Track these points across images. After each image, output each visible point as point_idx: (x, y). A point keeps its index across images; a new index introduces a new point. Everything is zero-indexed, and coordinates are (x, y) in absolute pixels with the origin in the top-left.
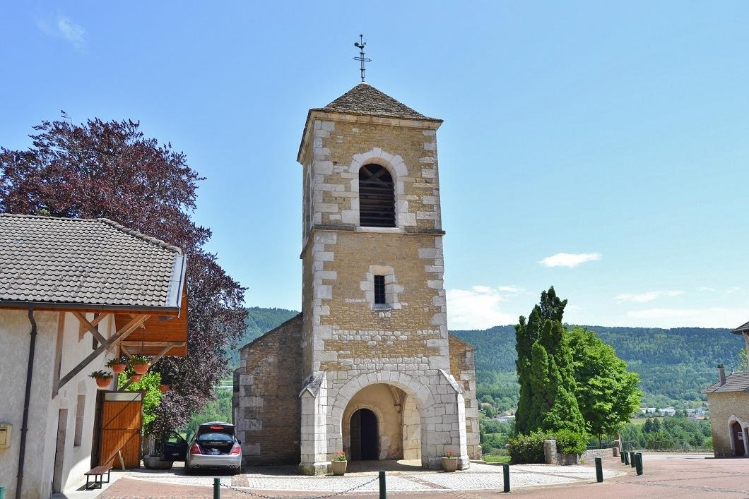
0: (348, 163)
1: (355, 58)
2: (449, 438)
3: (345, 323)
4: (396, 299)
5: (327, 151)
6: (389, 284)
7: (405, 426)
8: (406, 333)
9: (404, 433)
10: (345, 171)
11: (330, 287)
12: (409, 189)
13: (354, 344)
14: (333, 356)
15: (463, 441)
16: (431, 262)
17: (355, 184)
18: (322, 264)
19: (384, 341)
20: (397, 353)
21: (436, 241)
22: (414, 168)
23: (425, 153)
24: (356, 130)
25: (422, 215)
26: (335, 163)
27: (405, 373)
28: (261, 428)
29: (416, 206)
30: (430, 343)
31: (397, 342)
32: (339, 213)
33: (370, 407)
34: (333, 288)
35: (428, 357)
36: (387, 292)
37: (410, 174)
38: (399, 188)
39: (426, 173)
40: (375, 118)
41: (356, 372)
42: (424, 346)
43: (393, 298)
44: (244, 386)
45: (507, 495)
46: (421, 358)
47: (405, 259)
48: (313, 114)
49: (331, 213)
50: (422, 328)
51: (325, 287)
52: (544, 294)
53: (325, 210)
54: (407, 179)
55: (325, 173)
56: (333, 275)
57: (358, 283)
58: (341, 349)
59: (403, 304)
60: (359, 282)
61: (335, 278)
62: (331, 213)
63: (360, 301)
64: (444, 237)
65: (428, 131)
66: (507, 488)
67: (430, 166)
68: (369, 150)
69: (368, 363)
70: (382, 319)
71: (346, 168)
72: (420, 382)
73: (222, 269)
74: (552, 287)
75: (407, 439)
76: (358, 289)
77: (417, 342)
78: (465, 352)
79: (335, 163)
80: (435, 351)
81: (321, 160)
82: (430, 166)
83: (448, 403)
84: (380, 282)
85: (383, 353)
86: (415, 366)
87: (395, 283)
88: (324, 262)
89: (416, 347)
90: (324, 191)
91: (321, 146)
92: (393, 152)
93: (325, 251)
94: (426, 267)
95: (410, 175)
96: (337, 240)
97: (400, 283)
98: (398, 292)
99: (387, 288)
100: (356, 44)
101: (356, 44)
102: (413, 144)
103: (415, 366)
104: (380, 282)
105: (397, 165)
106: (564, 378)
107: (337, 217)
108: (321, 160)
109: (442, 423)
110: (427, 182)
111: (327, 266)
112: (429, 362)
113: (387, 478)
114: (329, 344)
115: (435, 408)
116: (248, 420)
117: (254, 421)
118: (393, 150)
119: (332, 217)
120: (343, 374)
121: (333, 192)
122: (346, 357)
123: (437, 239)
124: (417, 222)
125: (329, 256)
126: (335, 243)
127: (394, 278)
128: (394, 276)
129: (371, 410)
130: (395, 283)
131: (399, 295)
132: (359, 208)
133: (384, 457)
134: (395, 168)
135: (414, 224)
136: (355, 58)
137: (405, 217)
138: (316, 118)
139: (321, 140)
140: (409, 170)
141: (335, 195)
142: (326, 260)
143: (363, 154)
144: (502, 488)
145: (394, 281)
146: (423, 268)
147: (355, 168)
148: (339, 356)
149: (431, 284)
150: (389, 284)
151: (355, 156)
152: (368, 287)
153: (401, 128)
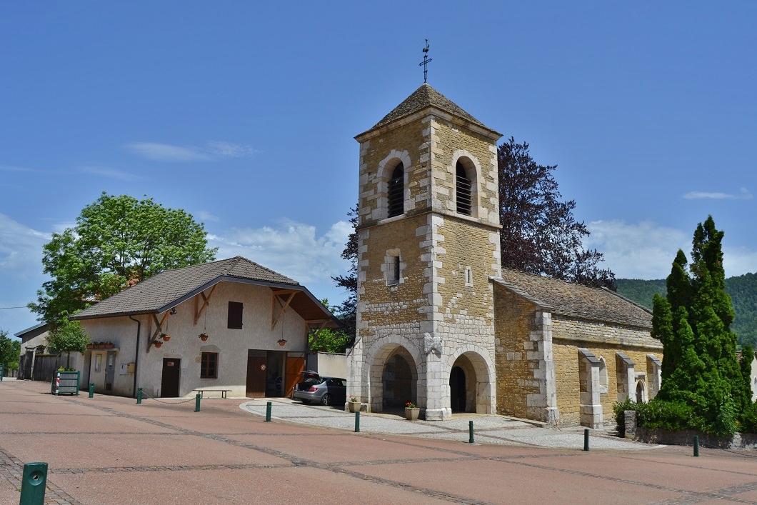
3: (373, 298)
8: (407, 303)
13: (377, 314)
15: (493, 392)
19: (393, 310)
20: (400, 320)
24: (381, 141)
25: (419, 198)
26: (369, 174)
30: (420, 310)
31: (401, 311)
32: (371, 213)
35: (419, 322)
40: (389, 126)
41: (377, 336)
42: (417, 312)
45: (268, 424)
50: (416, 298)
52: (700, 226)
56: (443, 251)
58: (370, 319)
66: (357, 429)
69: (383, 329)
70: (392, 293)
74: (710, 219)
75: (478, 395)
77: (413, 310)
78: (535, 312)
79: (369, 174)
85: (392, 320)
86: (410, 330)
103: (410, 330)
106: (697, 335)
111: (439, 243)
113: (361, 418)
117: (390, 373)
120: (370, 338)
125: (442, 238)
137: (409, 204)
144: (582, 446)
149: (423, 258)
153: (408, 125)
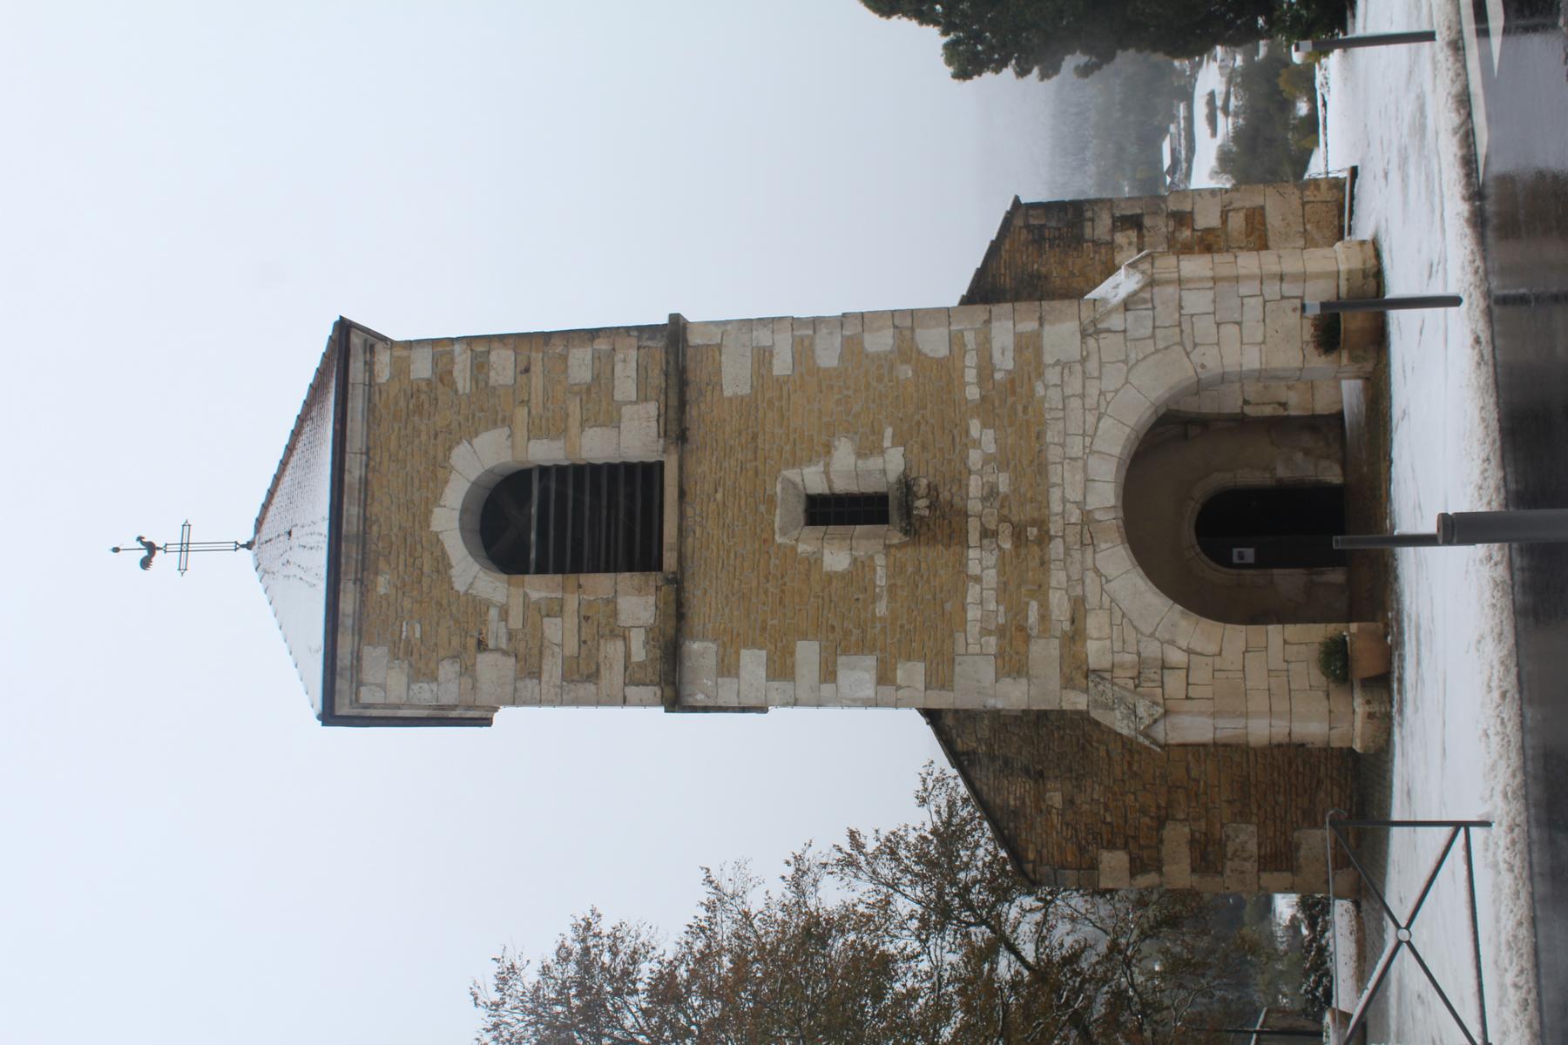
0: (479, 607)
1: (183, 570)
2: (1284, 303)
4: (875, 463)
5: (447, 670)
6: (829, 481)
7: (1248, 410)
9: (1268, 411)
10: (504, 614)
11: (841, 660)
12: (552, 427)
14: (1045, 653)
16: (763, 357)
17: (539, 588)
18: (776, 684)
21: (699, 342)
22: (486, 409)
23: (444, 376)
24: (382, 584)
26: (481, 645)
27: (1093, 437)
28: (1252, 828)
29: (599, 403)
30: (1005, 362)
33: (1192, 510)
34: (846, 652)
36: (853, 488)
37: (504, 420)
38: (546, 452)
39: (503, 366)
42: (1012, 383)
43: (869, 473)
44: (1132, 875)
46: (1048, 391)
47: (755, 437)
48: (343, 709)
49: (627, 655)
51: (842, 675)
53: (619, 679)
54: (521, 433)
55: (511, 674)
57: (831, 577)
59: (887, 443)
60: (828, 574)
61: (815, 645)
62: (627, 655)
63: (880, 572)
64: (691, 317)
65: (377, 368)
67: (480, 366)
68: (437, 541)
71: (493, 613)
72: (1117, 391)
73: (950, 70)
75: (1284, 405)
76: (846, 577)
79: (481, 645)
80: (1029, 347)
81: (474, 688)
82: (480, 366)
83: (1181, 307)
84: (826, 511)
87: (827, 465)
88: (770, 678)
89: (1013, 401)
90: (563, 678)
91: (434, 686)
92: (441, 473)
93: (737, 676)
94: (776, 372)
95: (508, 421)
96: (704, 638)
97: (828, 448)
98: (852, 459)
99: (842, 486)
100: (145, 563)
101: (145, 563)
102: (419, 409)
104: (826, 511)
105: (482, 456)
107: (637, 640)
108: (474, 688)
109: (1239, 324)
110: (527, 370)
112: (1058, 362)
114: (1012, 664)
115: (1195, 345)
116: (1229, 863)
118: (438, 471)
119: (639, 653)
121: (567, 653)
122: (1044, 617)
123: (694, 339)
124: (646, 400)
126: (712, 647)
127: (813, 469)
128: (806, 471)
129: (1199, 506)
130: (827, 465)
131: (860, 455)
132: (612, 575)
133: (1337, 469)
134: (473, 478)
135: (652, 408)
136: (183, 570)
138: (356, 700)
139: (415, 687)
140: (495, 424)
141: (572, 647)
142: (762, 673)
143: (453, 562)
145: (820, 467)
146: (780, 383)
147: (490, 586)
148: (1045, 632)
150: (829, 481)
151: (460, 586)
152: (836, 553)
